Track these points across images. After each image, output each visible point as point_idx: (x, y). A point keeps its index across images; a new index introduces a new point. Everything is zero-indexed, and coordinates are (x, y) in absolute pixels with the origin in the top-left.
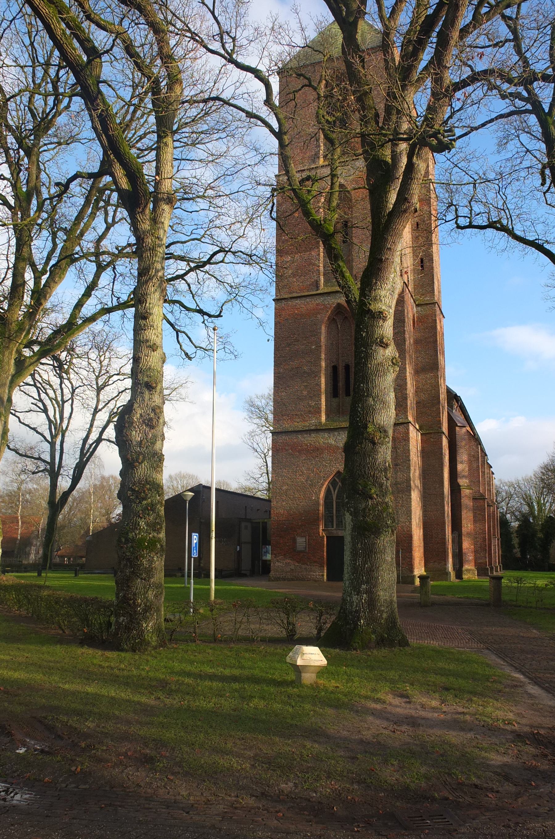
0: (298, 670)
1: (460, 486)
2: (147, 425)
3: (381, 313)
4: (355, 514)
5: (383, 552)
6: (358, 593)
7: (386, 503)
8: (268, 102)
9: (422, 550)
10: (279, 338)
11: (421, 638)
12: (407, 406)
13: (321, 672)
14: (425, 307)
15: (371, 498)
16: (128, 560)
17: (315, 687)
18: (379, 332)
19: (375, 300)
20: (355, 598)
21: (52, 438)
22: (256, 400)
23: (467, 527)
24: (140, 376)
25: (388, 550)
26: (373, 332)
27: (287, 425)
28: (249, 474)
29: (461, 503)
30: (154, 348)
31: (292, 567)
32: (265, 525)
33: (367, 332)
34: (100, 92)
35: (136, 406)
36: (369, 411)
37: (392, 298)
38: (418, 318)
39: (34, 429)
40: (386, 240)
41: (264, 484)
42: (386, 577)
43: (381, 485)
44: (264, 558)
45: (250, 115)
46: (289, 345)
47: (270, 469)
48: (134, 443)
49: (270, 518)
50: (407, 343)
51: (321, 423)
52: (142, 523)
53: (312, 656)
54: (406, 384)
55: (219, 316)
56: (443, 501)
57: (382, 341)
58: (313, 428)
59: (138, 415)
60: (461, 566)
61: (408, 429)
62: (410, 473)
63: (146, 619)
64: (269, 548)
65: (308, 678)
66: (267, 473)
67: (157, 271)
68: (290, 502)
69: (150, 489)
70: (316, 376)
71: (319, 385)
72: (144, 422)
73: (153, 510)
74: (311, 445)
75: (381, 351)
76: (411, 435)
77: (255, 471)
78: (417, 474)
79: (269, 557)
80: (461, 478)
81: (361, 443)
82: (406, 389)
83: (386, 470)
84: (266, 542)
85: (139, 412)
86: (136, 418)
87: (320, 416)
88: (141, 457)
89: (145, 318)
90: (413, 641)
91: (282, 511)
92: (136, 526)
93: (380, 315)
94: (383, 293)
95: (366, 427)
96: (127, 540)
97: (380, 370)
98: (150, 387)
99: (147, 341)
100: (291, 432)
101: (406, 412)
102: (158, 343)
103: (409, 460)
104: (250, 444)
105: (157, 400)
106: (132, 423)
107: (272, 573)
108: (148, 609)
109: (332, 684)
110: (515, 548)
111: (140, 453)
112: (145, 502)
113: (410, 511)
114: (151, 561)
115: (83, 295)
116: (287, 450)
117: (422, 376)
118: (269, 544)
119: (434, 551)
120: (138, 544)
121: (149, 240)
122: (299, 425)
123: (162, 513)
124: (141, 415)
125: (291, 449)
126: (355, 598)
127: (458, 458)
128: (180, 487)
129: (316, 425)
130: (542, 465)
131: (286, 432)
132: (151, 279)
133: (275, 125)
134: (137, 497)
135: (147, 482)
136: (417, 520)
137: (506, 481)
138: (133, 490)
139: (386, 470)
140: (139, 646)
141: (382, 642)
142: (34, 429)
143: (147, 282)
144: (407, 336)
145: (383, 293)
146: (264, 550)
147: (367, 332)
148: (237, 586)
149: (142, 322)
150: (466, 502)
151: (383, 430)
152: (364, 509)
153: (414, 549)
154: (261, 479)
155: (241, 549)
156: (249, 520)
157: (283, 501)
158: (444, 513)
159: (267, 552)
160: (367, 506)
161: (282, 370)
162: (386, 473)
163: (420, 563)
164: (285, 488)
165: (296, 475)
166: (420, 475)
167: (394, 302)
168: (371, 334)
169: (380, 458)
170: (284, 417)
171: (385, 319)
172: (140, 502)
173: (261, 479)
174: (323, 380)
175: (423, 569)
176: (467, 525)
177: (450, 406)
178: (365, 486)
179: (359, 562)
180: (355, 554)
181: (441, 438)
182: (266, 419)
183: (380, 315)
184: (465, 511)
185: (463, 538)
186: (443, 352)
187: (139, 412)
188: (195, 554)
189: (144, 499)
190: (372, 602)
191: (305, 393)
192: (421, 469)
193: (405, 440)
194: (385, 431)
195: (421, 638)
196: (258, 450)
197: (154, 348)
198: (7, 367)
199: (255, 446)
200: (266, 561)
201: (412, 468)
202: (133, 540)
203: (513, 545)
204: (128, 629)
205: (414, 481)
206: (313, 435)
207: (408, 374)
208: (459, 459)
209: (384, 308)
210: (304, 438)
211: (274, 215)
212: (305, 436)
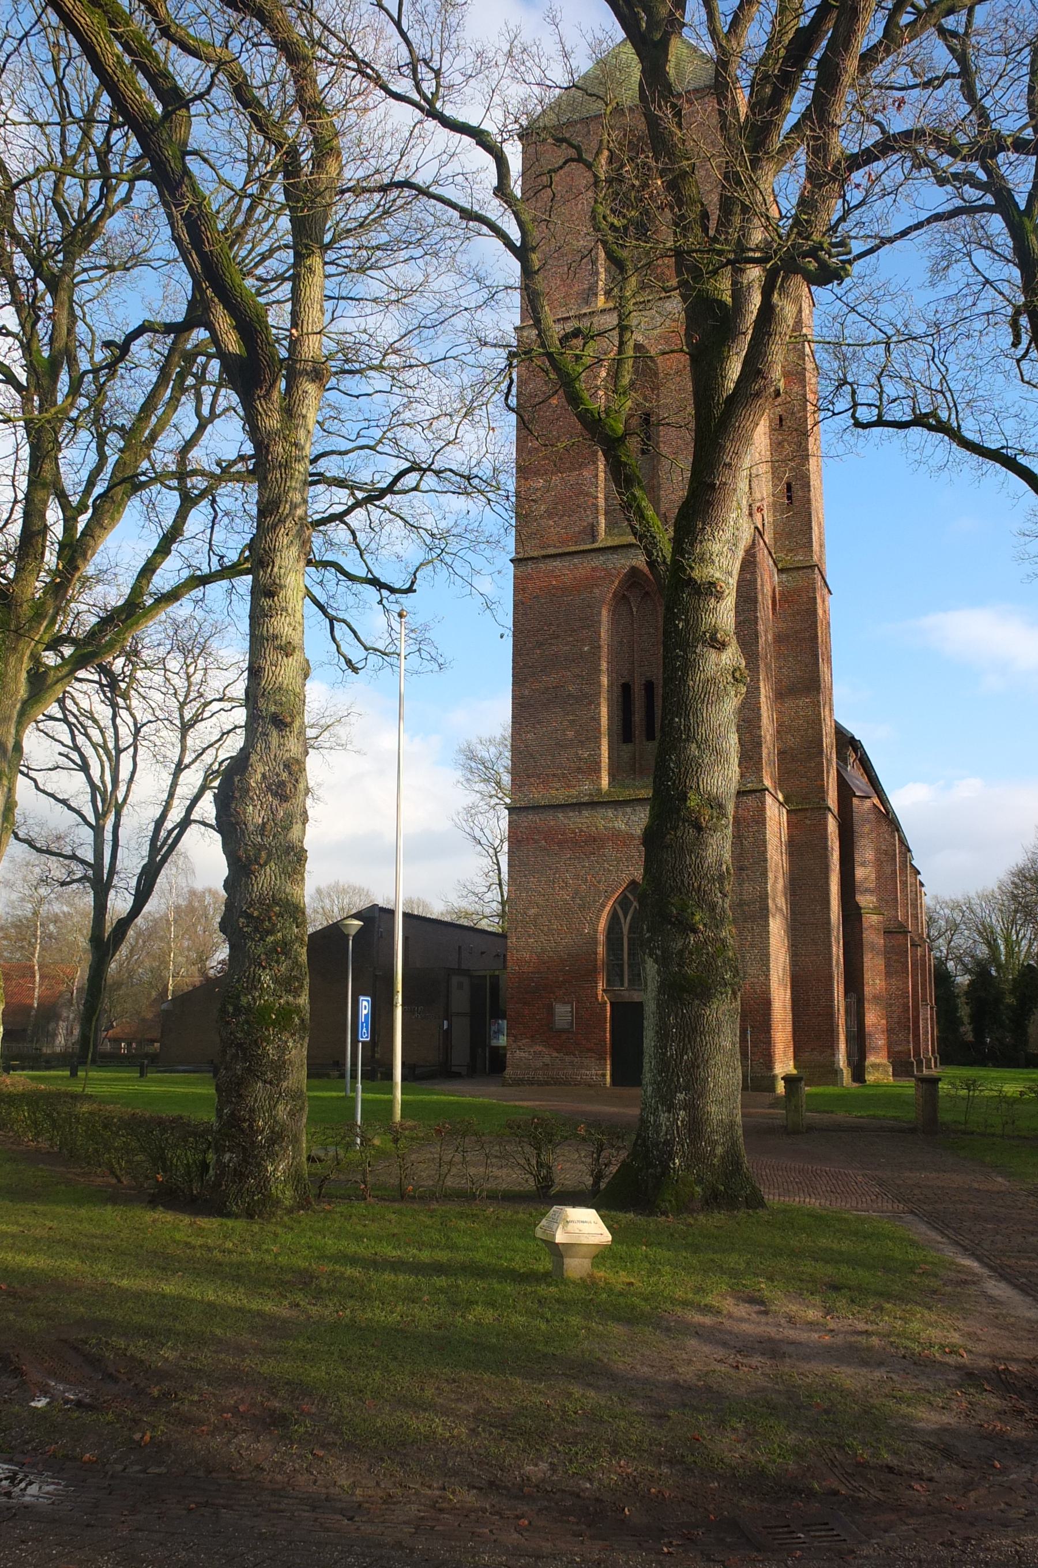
0: (558, 1252)
1: (860, 908)
2: (275, 795)
3: (712, 584)
4: (663, 961)
5: (717, 1031)
6: (670, 1108)
7: (723, 940)
8: (501, 190)
9: (789, 1029)
10: (522, 632)
11: (788, 1193)
12: (761, 758)
13: (601, 1255)
14: (795, 574)
15: (695, 931)
16: (240, 1046)
17: (588, 1284)
18: (708, 620)
19: (702, 560)
20: (663, 1117)
21: (97, 819)
22: (479, 747)
23: (874, 985)
24: (262, 703)
25: (726, 1029)
26: (698, 621)
27: (538, 795)
28: (465, 886)
29: (861, 939)
30: (288, 650)
31: (547, 1060)
32: (495, 981)
33: (687, 621)
34: (186, 172)
35: (254, 758)
36: (690, 768)
37: (733, 557)
38: (782, 593)
39: (64, 802)
40: (722, 448)
41: (494, 905)
42: (722, 1078)
43: (713, 907)
44: (494, 1043)
45: (467, 215)
46: (540, 645)
47: (505, 876)
48: (251, 828)
49: (505, 968)
50: (762, 641)
51: (599, 790)
52: (266, 978)
53: (584, 1226)
54: (759, 717)
55: (410, 590)
56: (829, 937)
57: (714, 638)
58: (586, 799)
59: (259, 776)
60: (863, 1057)
61: (763, 803)
62: (766, 883)
63: (273, 1156)
64: (504, 1023)
65: (576, 1267)
66: (500, 885)
67: (294, 507)
68: (543, 938)
69: (280, 915)
70: (590, 703)
71: (597, 720)
72: (269, 788)
73: (286, 953)
74: (581, 831)
75: (713, 655)
76: (768, 813)
77: (476, 879)
78: (780, 885)
79: (503, 1041)
80: (863, 893)
81: (675, 828)
82: (760, 727)
83: (721, 878)
84: (498, 1013)
85: (260, 769)
86: (254, 780)
87: (599, 778)
88: (263, 854)
89: (271, 594)
90: (773, 1199)
91: (527, 955)
92: (254, 983)
93: (711, 590)
94: (716, 547)
95: (684, 798)
96: (238, 1010)
97: (711, 691)
98: (280, 723)
99: (275, 637)
100: (544, 807)
101: (760, 770)
102: (296, 641)
103: (765, 860)
104: (468, 830)
105: (293, 747)
106: (246, 790)
107: (509, 1072)
108: (276, 1137)
109: (621, 1278)
110: (963, 1024)
111: (261, 847)
112: (270, 939)
113: (767, 955)
114: (283, 1049)
115: (156, 552)
116: (536, 842)
117: (789, 703)
118: (504, 1018)
119: (812, 1030)
120: (259, 1017)
121: (278, 449)
122: (559, 794)
123: (304, 958)
124: (264, 775)
125: (544, 838)
126: (663, 1117)
127: (856, 856)
128: (336, 910)
129: (591, 795)
130: (1015, 870)
131: (536, 808)
132: (282, 521)
133: (515, 234)
134: (256, 929)
135: (275, 901)
136: (781, 973)
137: (947, 899)
138: (249, 916)
139: (721, 878)
140: (259, 1207)
141: (714, 1200)
142: (64, 802)
143: (274, 527)
144: (761, 628)
145: (716, 547)
146: (494, 1028)
147: (687, 621)
148: (443, 1095)
149: (266, 602)
150: (872, 937)
151: (716, 804)
152: (681, 952)
153: (774, 1026)
154: (489, 896)
155: (450, 1025)
156: (466, 973)
157: (530, 937)
158: (830, 959)
159: (499, 1032)
160: (686, 946)
161: (527, 692)
162: (722, 883)
163: (785, 1052)
164: (532, 911)
165: (553, 889)
166: (785, 887)
167: (738, 565)
168: (693, 625)
169: (710, 855)
170: (532, 780)
171: (719, 597)
172: (262, 939)
173: (489, 896)
174: (604, 710)
175: (792, 1063)
176: (874, 982)
177: (842, 758)
178: (683, 909)
179: (672, 1051)
180: (663, 1035)
181: (826, 818)
182: (498, 783)
183: (711, 590)
184: (870, 956)
185: (866, 1005)
186: (829, 658)
187: (260, 769)
188: (365, 1036)
189: (270, 932)
190: (696, 1126)
191: (570, 734)
192: (787, 876)
193: (757, 823)
194: (721, 806)
195: (788, 1193)
196: (483, 841)
197: (288, 650)
198: (12, 686)
199: (478, 833)
200: (498, 1048)
201: (771, 875)
202: (249, 1010)
203: (960, 1018)
204: (240, 1175)
205: (774, 900)
206: (585, 813)
207: (763, 699)
208: (858, 858)
209: (717, 575)
210: (569, 818)
211: (513, 401)
212: (571, 814)
